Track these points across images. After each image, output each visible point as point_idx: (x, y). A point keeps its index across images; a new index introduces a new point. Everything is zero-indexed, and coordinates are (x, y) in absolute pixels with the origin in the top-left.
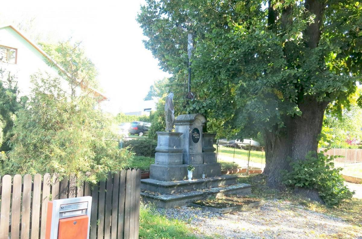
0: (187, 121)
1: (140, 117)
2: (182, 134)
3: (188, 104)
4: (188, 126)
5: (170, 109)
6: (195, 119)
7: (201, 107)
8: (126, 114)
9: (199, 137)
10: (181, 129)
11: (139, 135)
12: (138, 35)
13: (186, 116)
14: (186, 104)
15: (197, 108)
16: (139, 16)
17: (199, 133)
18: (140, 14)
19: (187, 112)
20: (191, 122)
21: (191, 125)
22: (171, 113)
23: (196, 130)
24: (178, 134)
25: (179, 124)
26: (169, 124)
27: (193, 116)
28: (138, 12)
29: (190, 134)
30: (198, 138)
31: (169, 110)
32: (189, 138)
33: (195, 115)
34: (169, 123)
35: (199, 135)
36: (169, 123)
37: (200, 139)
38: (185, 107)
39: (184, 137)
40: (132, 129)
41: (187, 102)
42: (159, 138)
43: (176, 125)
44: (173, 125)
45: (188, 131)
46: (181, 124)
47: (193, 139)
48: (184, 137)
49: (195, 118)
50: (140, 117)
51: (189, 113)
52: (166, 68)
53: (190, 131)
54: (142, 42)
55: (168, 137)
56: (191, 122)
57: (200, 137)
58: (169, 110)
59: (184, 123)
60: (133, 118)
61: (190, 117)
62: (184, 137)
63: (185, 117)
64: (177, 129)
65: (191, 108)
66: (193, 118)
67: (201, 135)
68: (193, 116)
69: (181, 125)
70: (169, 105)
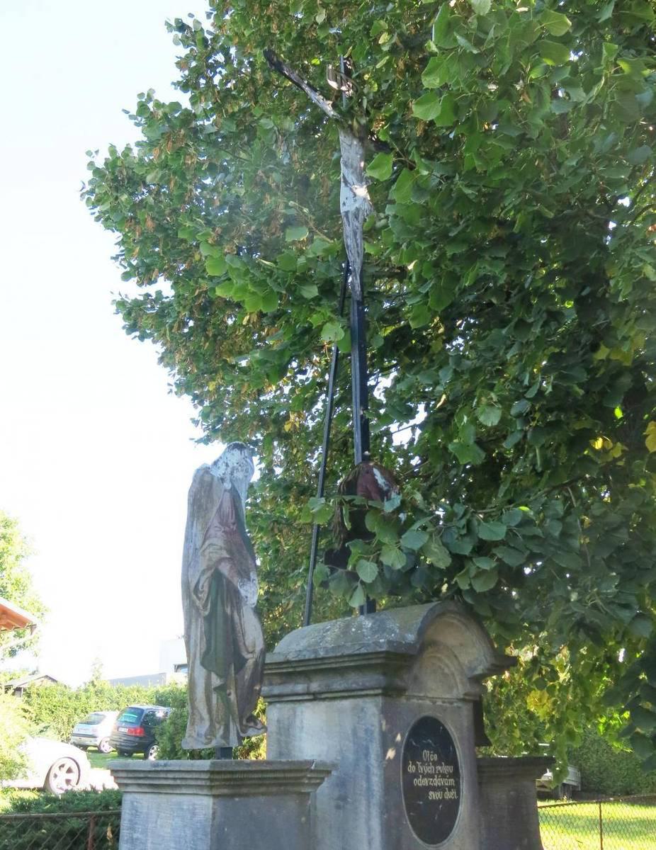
0: (363, 663)
1: (157, 692)
2: (323, 771)
3: (358, 532)
4: (371, 709)
5: (225, 569)
6: (425, 644)
7: (467, 549)
8: (113, 682)
9: (457, 788)
10: (313, 731)
11: (146, 757)
12: (93, 264)
13: (348, 626)
14: (350, 536)
15: (438, 558)
16: (97, 171)
17: (453, 761)
18: (100, 164)
19: (358, 601)
20: (392, 670)
21: (391, 692)
22: (235, 598)
23: (427, 735)
24: (290, 778)
25: (300, 688)
26: (221, 689)
27: (401, 625)
28: (89, 153)
29: (388, 766)
30: (450, 795)
31: (217, 577)
32: (385, 808)
33: (418, 613)
34: (216, 681)
35: (456, 774)
36: (216, 681)
37: (463, 809)
38: (337, 559)
39: (342, 801)
40: (125, 735)
41: (358, 516)
42: (135, 812)
43: (275, 699)
44: (248, 699)
45: (375, 748)
46: (315, 686)
47: (410, 808)
48: (343, 798)
49: (421, 632)
50: (157, 692)
51: (370, 607)
52: (224, 443)
53: (386, 743)
54: (114, 307)
55: (204, 805)
56: (392, 670)
57: (464, 787)
58: (217, 577)
59: (338, 684)
60: (135, 694)
61: (380, 628)
62: (343, 798)
63: (345, 631)
64: (285, 732)
65: (394, 559)
66: (411, 637)
67: (464, 771)
68: (401, 625)
69: (316, 697)
70: (218, 540)
